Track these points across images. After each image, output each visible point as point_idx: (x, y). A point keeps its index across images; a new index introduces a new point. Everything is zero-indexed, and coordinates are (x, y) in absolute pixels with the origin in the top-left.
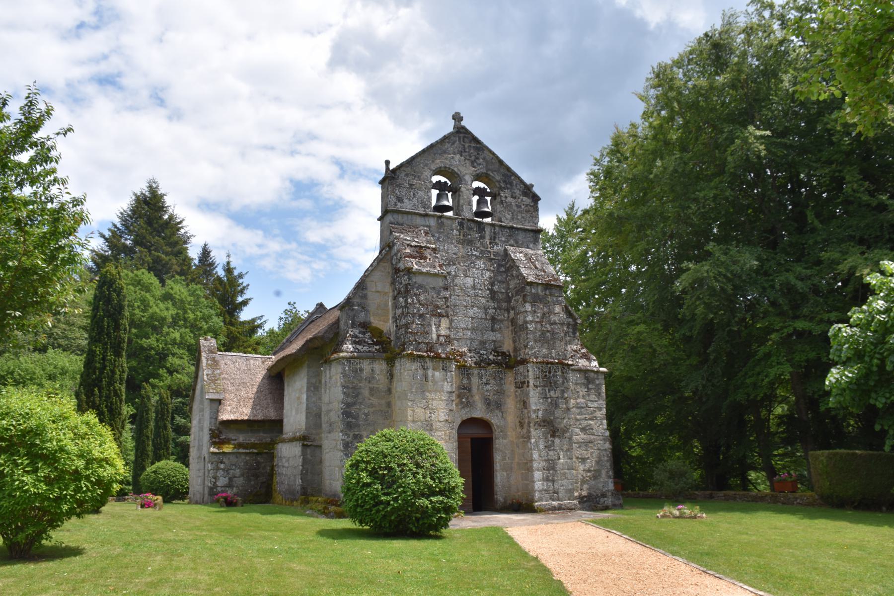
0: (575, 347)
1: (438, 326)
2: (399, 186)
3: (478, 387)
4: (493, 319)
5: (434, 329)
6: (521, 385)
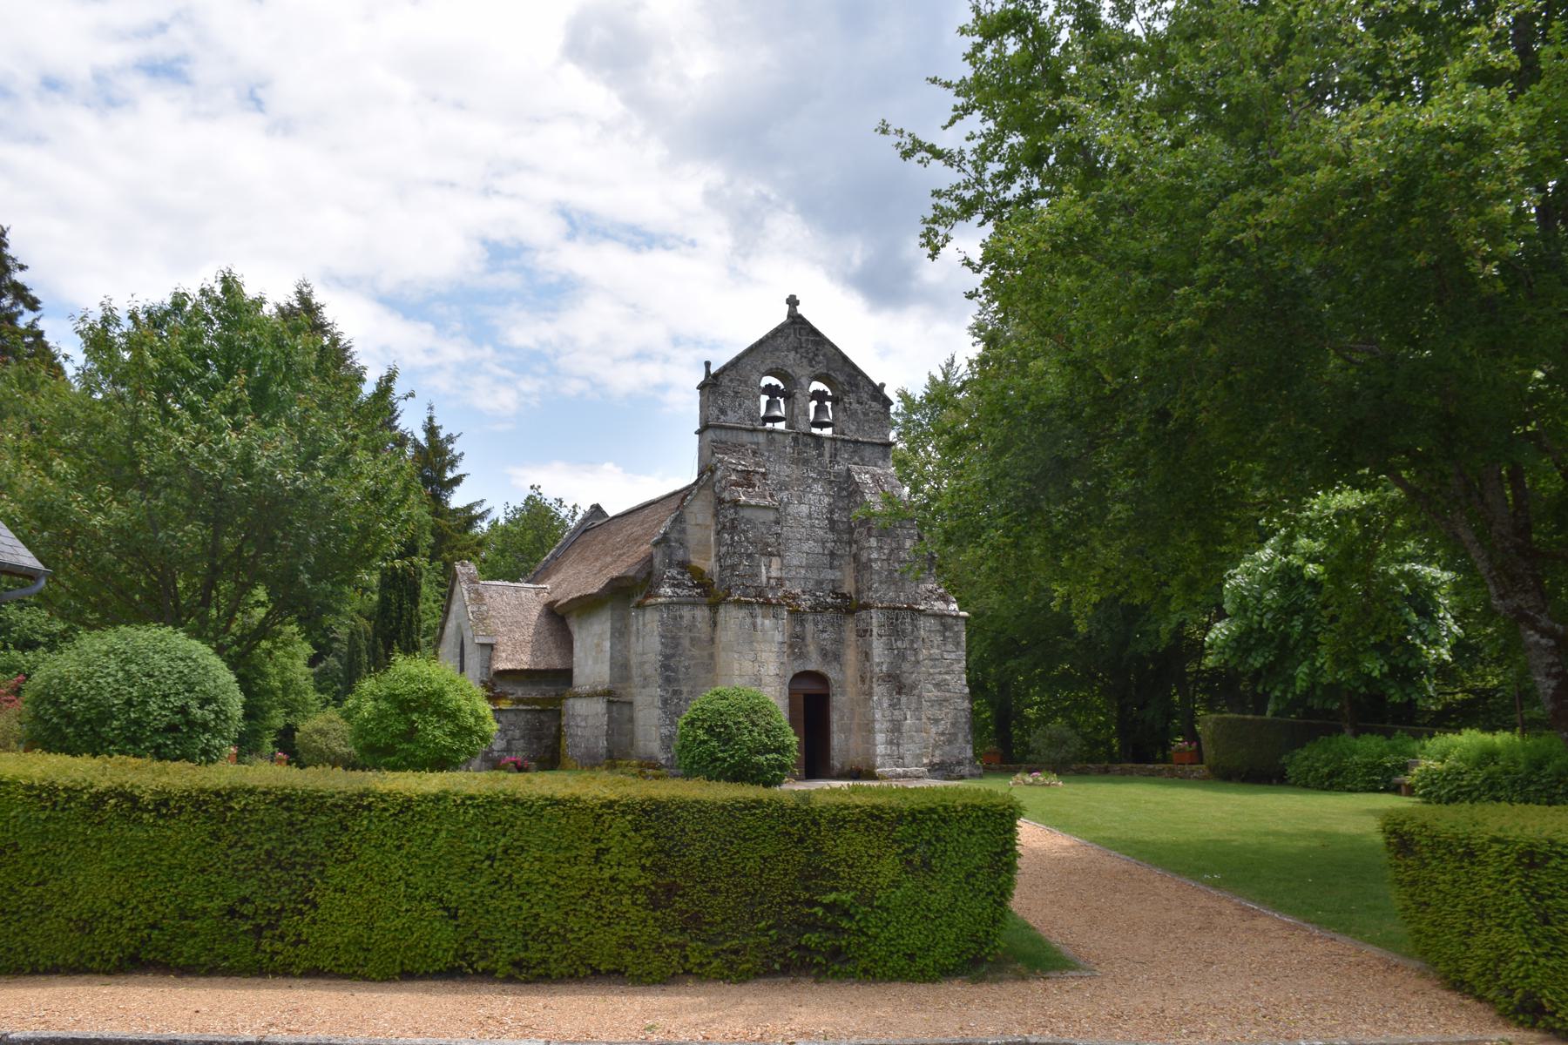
0: (930, 587)
1: (768, 567)
2: (723, 394)
4: (832, 554)
5: (764, 571)
6: (864, 633)
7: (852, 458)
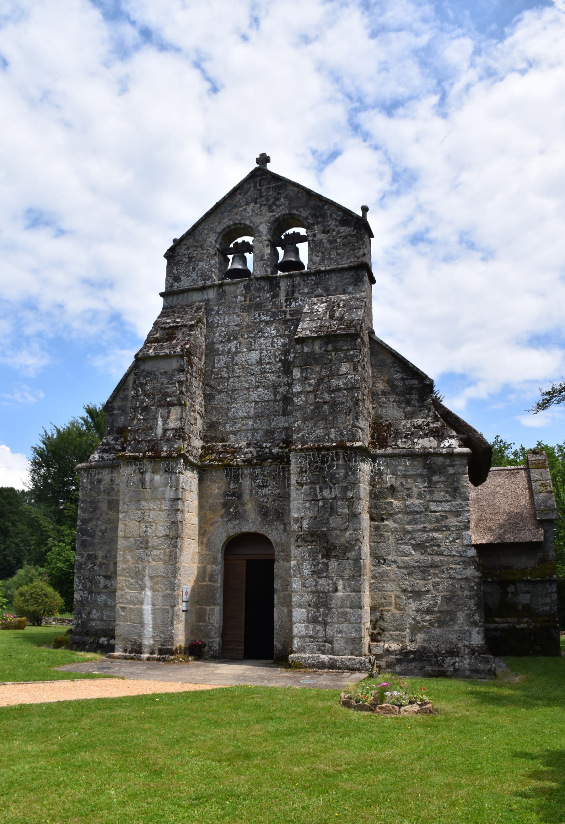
1: (166, 419)
3: (251, 491)
7: (314, 290)
